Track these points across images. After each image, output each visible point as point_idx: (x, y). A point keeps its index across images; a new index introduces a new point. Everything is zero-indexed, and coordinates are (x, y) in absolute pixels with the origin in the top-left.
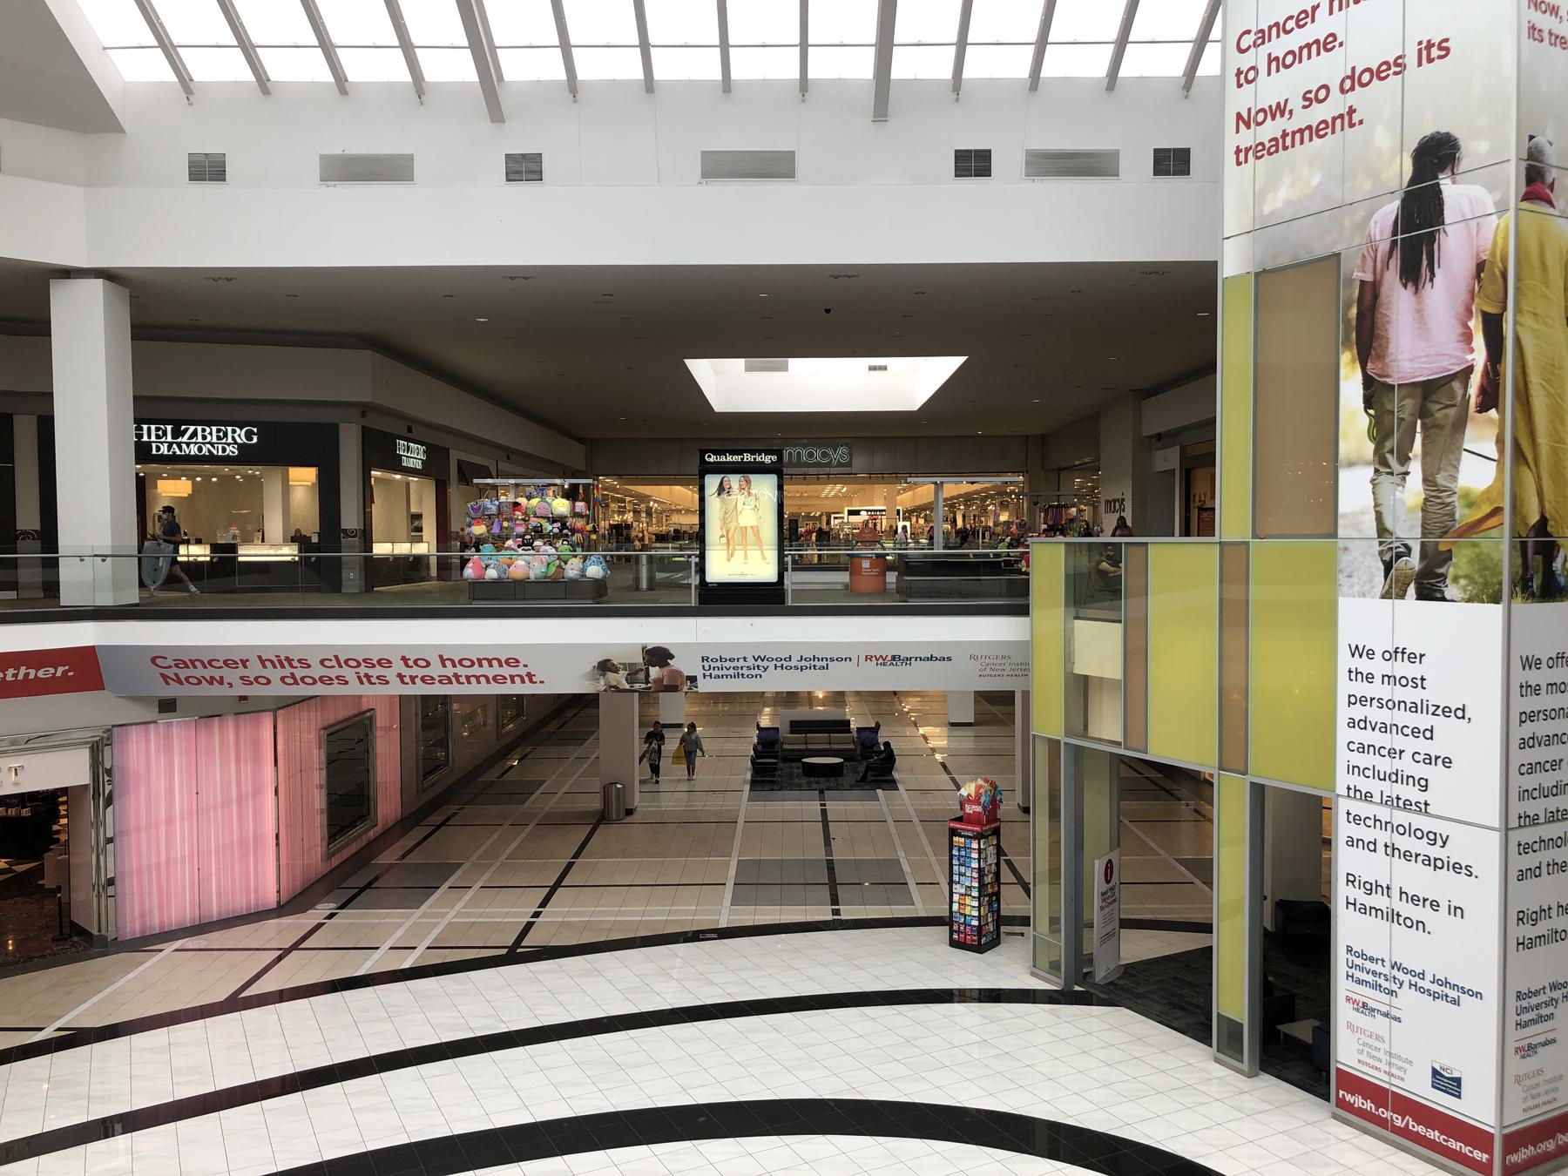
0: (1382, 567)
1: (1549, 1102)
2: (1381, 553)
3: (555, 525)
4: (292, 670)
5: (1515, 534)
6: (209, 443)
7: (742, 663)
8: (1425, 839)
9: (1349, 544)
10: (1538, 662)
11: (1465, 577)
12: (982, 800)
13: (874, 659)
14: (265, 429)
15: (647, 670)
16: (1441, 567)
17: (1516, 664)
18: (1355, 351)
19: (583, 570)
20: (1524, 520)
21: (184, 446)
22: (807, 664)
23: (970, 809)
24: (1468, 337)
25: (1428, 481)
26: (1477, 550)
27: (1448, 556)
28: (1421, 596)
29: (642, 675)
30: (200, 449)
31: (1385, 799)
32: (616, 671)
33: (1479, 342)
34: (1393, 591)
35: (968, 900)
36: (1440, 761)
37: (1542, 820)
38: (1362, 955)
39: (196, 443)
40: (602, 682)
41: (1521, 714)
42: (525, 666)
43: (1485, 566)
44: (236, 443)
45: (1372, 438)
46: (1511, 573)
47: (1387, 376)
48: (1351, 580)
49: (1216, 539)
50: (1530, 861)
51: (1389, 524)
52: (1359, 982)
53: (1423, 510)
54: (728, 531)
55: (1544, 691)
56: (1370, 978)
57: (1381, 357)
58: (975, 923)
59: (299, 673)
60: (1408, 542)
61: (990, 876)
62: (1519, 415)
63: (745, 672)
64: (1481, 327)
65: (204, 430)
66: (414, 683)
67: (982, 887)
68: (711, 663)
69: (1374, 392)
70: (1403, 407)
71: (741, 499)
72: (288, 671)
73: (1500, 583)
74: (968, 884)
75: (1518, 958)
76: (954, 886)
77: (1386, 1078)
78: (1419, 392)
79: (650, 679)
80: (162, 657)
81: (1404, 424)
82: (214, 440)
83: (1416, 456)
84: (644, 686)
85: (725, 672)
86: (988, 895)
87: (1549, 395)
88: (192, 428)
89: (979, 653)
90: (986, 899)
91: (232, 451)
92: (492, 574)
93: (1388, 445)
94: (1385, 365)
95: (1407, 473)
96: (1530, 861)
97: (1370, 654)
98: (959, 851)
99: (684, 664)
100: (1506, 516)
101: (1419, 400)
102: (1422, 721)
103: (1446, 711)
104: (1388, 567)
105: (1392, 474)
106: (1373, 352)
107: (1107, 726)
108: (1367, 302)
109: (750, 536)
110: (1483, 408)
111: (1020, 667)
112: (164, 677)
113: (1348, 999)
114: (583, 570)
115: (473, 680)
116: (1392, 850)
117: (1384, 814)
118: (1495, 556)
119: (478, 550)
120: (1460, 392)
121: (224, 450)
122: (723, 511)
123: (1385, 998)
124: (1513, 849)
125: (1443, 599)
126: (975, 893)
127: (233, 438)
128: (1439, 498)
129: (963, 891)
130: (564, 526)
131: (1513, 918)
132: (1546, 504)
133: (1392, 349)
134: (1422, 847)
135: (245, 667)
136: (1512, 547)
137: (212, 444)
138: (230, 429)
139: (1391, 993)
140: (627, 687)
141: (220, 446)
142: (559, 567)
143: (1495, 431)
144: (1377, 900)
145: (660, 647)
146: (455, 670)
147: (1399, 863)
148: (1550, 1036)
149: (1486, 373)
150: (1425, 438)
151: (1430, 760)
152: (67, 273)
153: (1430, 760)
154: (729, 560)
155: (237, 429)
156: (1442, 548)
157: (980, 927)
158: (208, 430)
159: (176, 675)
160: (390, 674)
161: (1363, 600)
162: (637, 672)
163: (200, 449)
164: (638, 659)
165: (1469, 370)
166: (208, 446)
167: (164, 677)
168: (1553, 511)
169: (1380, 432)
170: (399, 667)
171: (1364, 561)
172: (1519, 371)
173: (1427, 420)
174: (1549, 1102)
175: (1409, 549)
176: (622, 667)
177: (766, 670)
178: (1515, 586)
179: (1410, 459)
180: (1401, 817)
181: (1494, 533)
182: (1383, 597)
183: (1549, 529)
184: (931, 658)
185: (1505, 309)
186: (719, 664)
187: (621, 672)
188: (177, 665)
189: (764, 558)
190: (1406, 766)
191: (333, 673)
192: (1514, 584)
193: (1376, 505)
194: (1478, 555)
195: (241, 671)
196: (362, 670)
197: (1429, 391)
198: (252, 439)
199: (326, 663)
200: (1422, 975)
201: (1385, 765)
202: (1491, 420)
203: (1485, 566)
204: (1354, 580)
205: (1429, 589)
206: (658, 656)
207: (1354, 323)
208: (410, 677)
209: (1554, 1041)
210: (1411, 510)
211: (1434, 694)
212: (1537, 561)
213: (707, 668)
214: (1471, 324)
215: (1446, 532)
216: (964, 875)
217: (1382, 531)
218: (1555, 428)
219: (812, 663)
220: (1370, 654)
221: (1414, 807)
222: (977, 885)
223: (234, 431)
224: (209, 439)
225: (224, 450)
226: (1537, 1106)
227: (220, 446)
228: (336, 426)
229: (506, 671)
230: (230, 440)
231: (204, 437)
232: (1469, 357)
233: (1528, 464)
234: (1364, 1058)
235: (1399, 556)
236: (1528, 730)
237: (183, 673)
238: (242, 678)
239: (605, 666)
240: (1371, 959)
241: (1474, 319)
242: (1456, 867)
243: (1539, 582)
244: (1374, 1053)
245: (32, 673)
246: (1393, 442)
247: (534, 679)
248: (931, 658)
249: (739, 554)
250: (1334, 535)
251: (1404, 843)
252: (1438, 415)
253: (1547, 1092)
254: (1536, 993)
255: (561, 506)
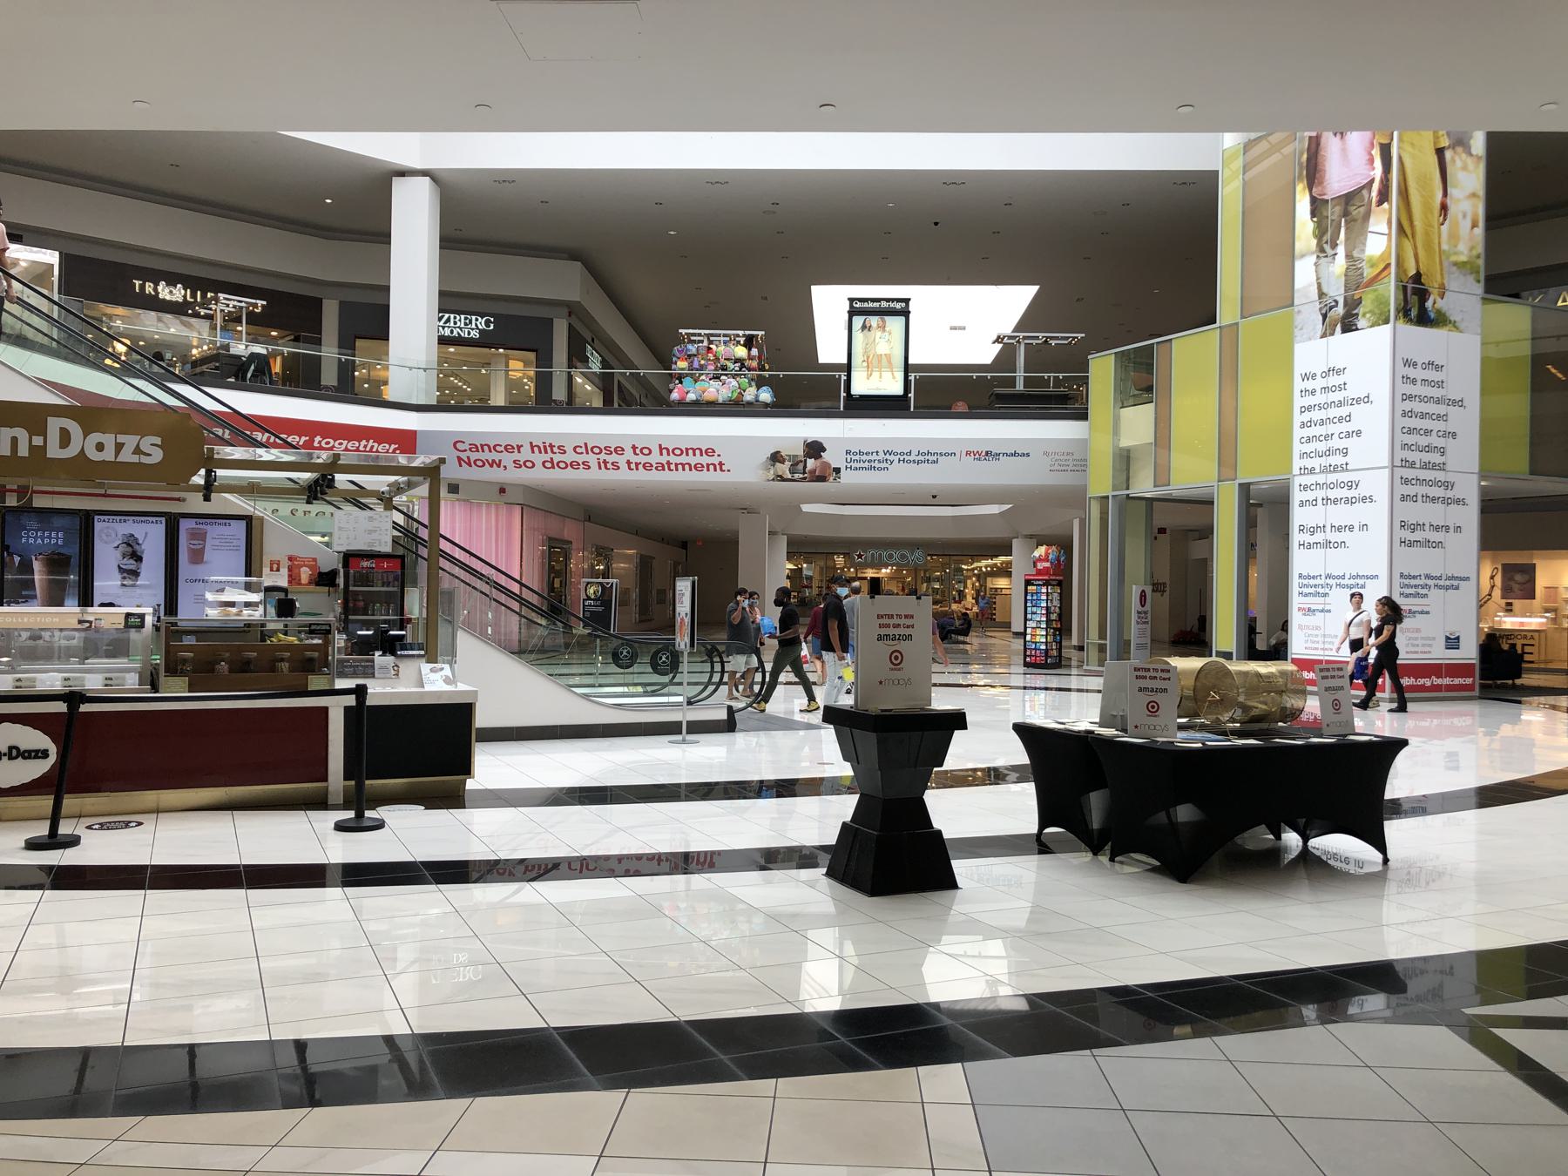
0: (1321, 318)
1: (1425, 653)
2: (1321, 309)
3: (737, 365)
4: (552, 456)
5: (1399, 279)
6: (459, 327)
7: (874, 457)
8: (1346, 487)
9: (1300, 308)
10: (1415, 364)
11: (1370, 312)
12: (1050, 558)
13: (972, 454)
14: (500, 320)
15: (806, 460)
16: (1355, 309)
17: (1400, 363)
18: (1305, 182)
19: (757, 396)
20: (1405, 272)
21: (441, 328)
22: (922, 458)
23: (1040, 566)
24: (1371, 161)
25: (1349, 256)
26: (1376, 293)
27: (1359, 302)
28: (1345, 330)
29: (801, 466)
30: (452, 332)
31: (1323, 468)
32: (783, 462)
33: (1378, 163)
34: (1328, 332)
35: (1038, 632)
36: (1355, 434)
37: (1418, 466)
38: (1309, 577)
39: (449, 327)
40: (772, 472)
41: (1403, 394)
42: (719, 455)
43: (1382, 302)
44: (478, 328)
45: (1315, 236)
46: (1396, 302)
47: (1324, 195)
48: (1301, 331)
49: (1217, 325)
50: (1410, 490)
51: (1325, 290)
52: (1306, 595)
53: (1346, 275)
54: (868, 358)
55: (1419, 383)
56: (1312, 590)
57: (1321, 183)
58: (1043, 647)
59: (557, 458)
60: (1336, 298)
61: (1055, 615)
62: (1402, 207)
63: (877, 465)
64: (1379, 153)
65: (455, 318)
66: (637, 469)
67: (1048, 621)
68: (852, 456)
69: (1317, 206)
70: (1333, 212)
71: (879, 334)
72: (547, 457)
73: (1389, 311)
74: (1038, 619)
75: (1401, 551)
76: (1028, 622)
77: (1321, 653)
78: (1343, 201)
79: (807, 470)
80: (461, 442)
81: (1334, 223)
82: (462, 325)
83: (1341, 242)
84: (801, 476)
85: (862, 465)
86: (1054, 628)
87: (1422, 196)
88: (447, 316)
89: (1049, 449)
90: (1052, 631)
91: (475, 334)
92: (691, 397)
93: (1325, 239)
94: (1324, 187)
95: (1336, 254)
96: (1410, 490)
97: (1314, 376)
98: (1032, 596)
99: (832, 457)
100: (1393, 268)
101: (1343, 207)
102: (1343, 411)
103: (1358, 401)
104: (1325, 316)
105: (1327, 256)
106: (1316, 181)
107: (1144, 486)
108: (1313, 150)
109: (884, 360)
110: (1380, 203)
111: (1080, 463)
112: (459, 459)
113: (1299, 609)
114: (757, 396)
115: (680, 467)
116: (1326, 500)
117: (1321, 479)
118: (1387, 295)
119: (681, 382)
120: (1366, 196)
121: (469, 333)
122: (864, 344)
123: (1321, 600)
124: (1397, 481)
125: (1357, 329)
126: (1044, 626)
127: (476, 325)
128: (1355, 265)
129: (1034, 625)
130: (743, 366)
131: (1397, 525)
132: (1421, 264)
133: (1327, 177)
134: (1345, 493)
135: (519, 452)
136: (1397, 287)
137: (461, 329)
138: (474, 318)
139: (1325, 595)
140: (790, 476)
141: (466, 330)
142: (740, 393)
143: (1387, 216)
144: (1319, 537)
145: (816, 442)
146: (668, 458)
147: (1331, 507)
148: (1426, 609)
149: (1382, 181)
150: (1347, 229)
151: (1349, 435)
152: (403, 173)
153: (1349, 435)
154: (868, 379)
155: (480, 319)
156: (1355, 297)
157: (1047, 651)
158: (458, 316)
159: (468, 458)
160: (622, 461)
161: (1309, 342)
162: (797, 464)
163: (452, 332)
164: (800, 452)
165: (1372, 181)
166: (458, 329)
167: (459, 459)
168: (1425, 270)
169: (1320, 232)
170: (629, 454)
171: (1308, 314)
172: (1402, 177)
173: (1348, 218)
174: (1425, 653)
175: (1336, 302)
176: (787, 458)
177: (892, 463)
178: (1399, 313)
179: (1337, 245)
180: (1332, 478)
181: (1386, 280)
182: (1322, 337)
183: (1422, 280)
184: (1014, 454)
185: (1392, 139)
186: (857, 457)
187: (787, 463)
188: (470, 449)
189: (894, 378)
190: (1336, 443)
191: (580, 459)
192: (1398, 311)
193: (1318, 279)
194: (1377, 297)
195: (516, 456)
196: (603, 456)
197: (1349, 199)
198: (490, 326)
199: (578, 450)
200: (1343, 577)
201: (1322, 446)
202: (1385, 210)
203: (1382, 302)
204: (1304, 331)
205: (1348, 326)
206: (815, 449)
207: (1305, 164)
208: (636, 463)
209: (1428, 613)
210: (1339, 277)
211: (1352, 392)
212: (1414, 300)
213: (849, 461)
214: (1373, 152)
215: (1358, 287)
216: (1035, 613)
217: (1321, 294)
218: (1427, 218)
219: (927, 457)
220: (1314, 376)
221: (1339, 469)
222: (1045, 619)
223: (477, 320)
224: (458, 325)
225: (469, 333)
226: (1416, 652)
227: (466, 330)
228: (552, 319)
229: (705, 460)
230: (474, 326)
231: (455, 323)
232: (1372, 173)
233: (1407, 236)
234: (1309, 645)
235: (1331, 308)
236: (1408, 406)
237: (474, 456)
238: (514, 462)
239: (776, 458)
240: (1314, 577)
241: (1375, 150)
242: (1364, 499)
243: (1416, 313)
244: (1315, 639)
245: (376, 445)
246: (1328, 236)
247: (724, 467)
248: (1014, 454)
249: (876, 375)
250: (1292, 305)
251: (1333, 494)
252: (1354, 213)
253: (1423, 645)
254: (1414, 577)
255: (741, 352)
